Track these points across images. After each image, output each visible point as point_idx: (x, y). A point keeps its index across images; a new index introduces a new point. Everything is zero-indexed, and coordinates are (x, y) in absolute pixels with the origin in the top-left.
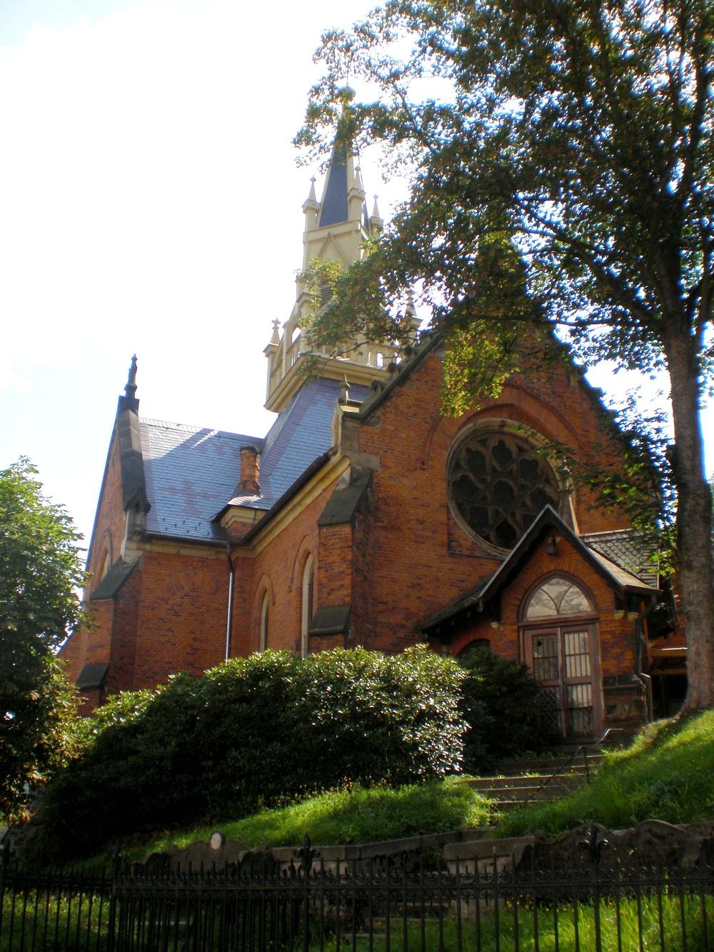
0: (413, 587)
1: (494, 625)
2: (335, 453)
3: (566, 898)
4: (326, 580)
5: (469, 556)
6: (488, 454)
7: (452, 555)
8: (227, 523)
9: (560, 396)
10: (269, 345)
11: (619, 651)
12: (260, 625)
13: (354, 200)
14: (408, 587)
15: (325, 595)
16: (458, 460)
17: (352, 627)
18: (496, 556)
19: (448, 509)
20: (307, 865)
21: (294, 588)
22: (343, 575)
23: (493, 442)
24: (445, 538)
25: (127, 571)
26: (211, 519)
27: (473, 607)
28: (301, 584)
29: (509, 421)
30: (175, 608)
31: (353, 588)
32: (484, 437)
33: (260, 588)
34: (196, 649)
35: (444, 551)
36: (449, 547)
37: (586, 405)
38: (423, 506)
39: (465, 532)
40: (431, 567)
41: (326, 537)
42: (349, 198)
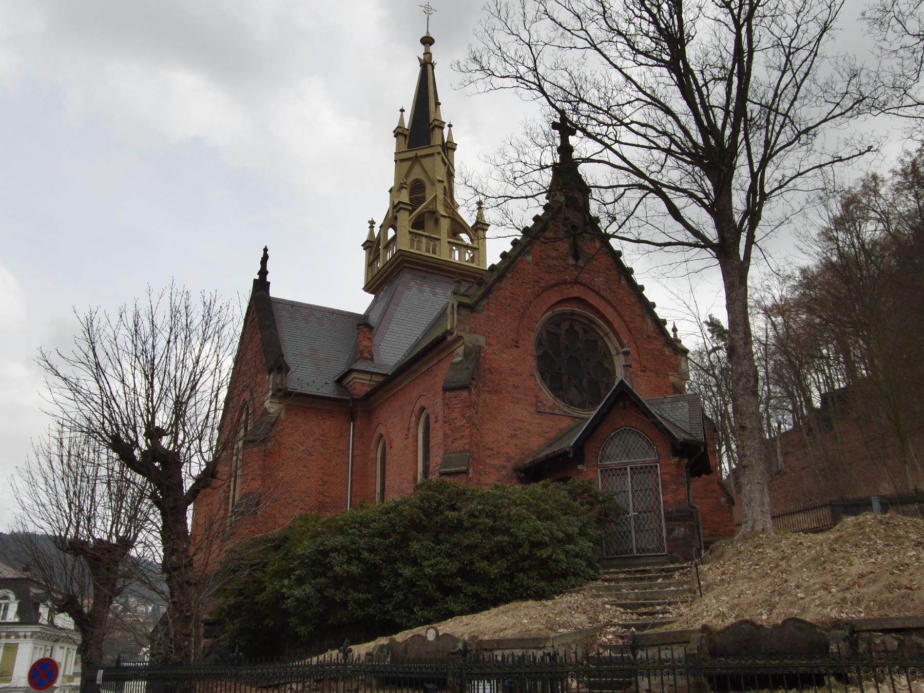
0: (511, 437)
1: (580, 467)
4: (450, 432)
5: (551, 414)
7: (540, 413)
8: (348, 383)
9: (614, 292)
17: (471, 468)
25: (273, 420)
26: (335, 379)
27: (565, 453)
28: (417, 433)
34: (325, 482)
35: (532, 410)
37: (633, 299)
40: (524, 422)
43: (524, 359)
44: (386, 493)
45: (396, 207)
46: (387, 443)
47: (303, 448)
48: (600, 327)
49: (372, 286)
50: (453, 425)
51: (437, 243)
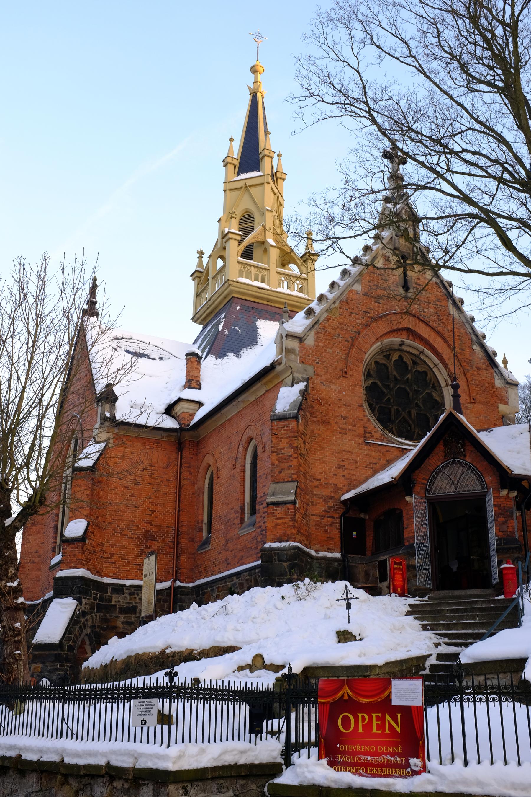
0: (339, 467)
1: (408, 499)
2: (280, 364)
4: (277, 462)
6: (391, 366)
9: (443, 323)
10: (196, 271)
11: (504, 519)
12: (203, 493)
13: (266, 158)
14: (336, 467)
15: (277, 473)
16: (369, 370)
19: (364, 408)
20: (171, 680)
22: (291, 458)
23: (395, 357)
24: (362, 431)
28: (245, 463)
29: (407, 341)
30: (137, 479)
32: (388, 353)
33: (204, 464)
35: (361, 440)
38: (345, 405)
39: (375, 425)
40: (352, 453)
41: (277, 429)
42: (261, 156)
43: (353, 389)
46: (214, 473)
47: (131, 477)
49: (198, 319)
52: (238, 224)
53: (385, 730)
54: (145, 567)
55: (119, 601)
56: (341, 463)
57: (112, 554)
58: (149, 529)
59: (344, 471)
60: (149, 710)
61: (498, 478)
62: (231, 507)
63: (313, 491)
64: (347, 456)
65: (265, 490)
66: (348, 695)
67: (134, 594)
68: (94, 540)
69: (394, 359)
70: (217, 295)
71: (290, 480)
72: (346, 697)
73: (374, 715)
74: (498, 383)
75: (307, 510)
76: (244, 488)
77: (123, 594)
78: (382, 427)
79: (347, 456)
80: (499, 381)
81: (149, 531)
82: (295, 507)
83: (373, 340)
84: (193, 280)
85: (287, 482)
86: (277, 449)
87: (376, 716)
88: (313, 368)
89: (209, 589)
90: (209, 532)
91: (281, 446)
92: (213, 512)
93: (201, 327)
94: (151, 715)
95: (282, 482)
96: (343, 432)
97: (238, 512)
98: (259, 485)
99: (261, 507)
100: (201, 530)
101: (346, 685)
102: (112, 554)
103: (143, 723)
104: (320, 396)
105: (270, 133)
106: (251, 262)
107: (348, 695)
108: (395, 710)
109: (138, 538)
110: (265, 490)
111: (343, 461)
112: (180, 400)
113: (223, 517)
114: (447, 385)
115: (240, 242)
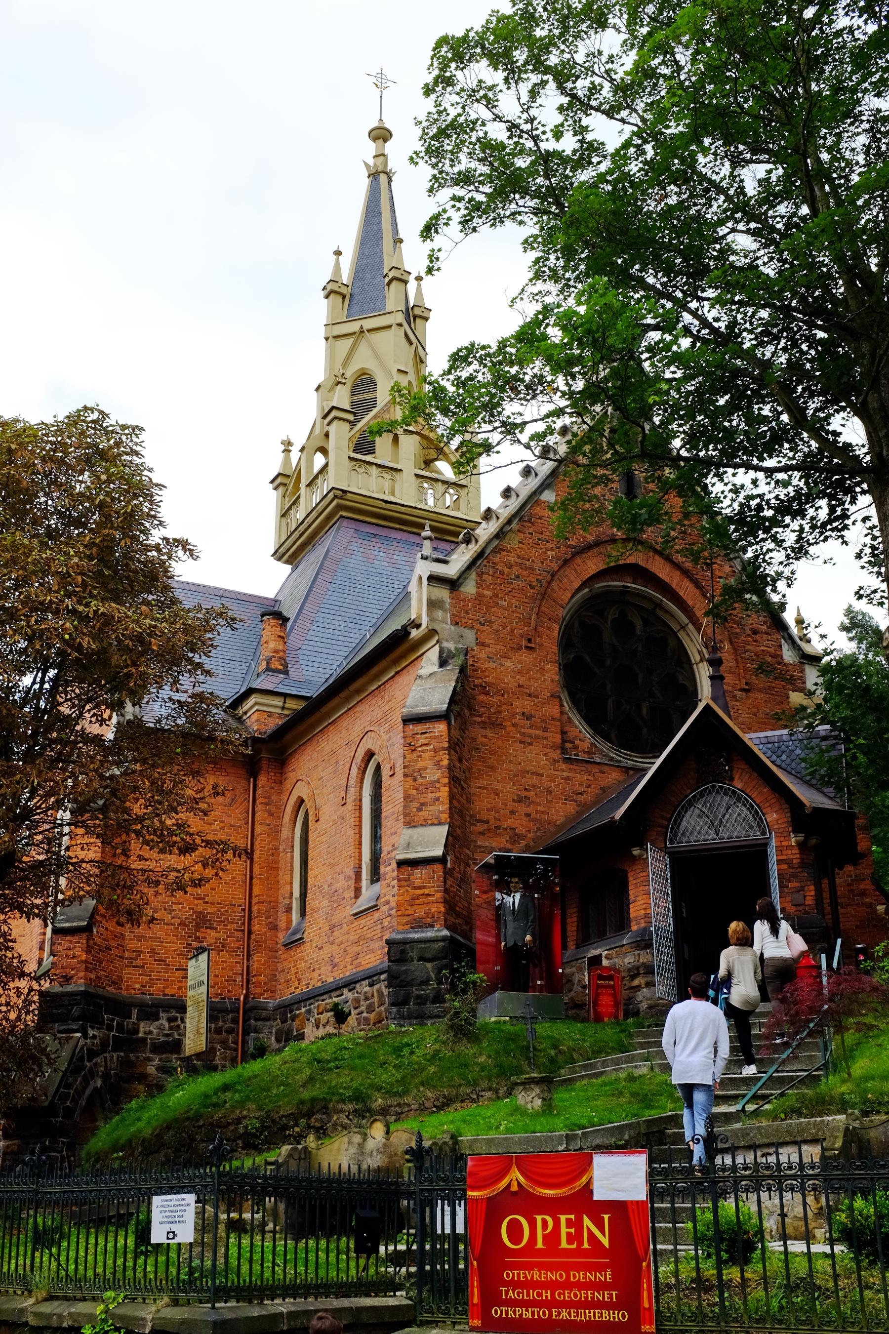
0: (520, 800)
1: (636, 852)
3: (359, 1182)
4: (414, 792)
7: (567, 760)
10: (279, 475)
11: (798, 884)
18: (620, 761)
19: (561, 700)
21: (350, 799)
22: (437, 785)
24: (558, 739)
28: (361, 795)
31: (451, 802)
35: (556, 755)
36: (564, 750)
38: (530, 695)
39: (581, 729)
40: (542, 776)
44: (309, 896)
45: (329, 414)
48: (672, 616)
49: (284, 554)
50: (419, 781)
51: (397, 476)
52: (349, 394)
53: (583, 1244)
54: (191, 972)
55: (150, 1032)
56: (524, 794)
57: (138, 953)
58: (200, 908)
59: (528, 806)
60: (180, 1213)
61: (788, 815)
62: (338, 869)
63: (476, 842)
64: (534, 780)
65: (393, 839)
66: (519, 1184)
67: (175, 1019)
68: (107, 929)
69: (610, 617)
70: (314, 514)
71: (436, 822)
72: (514, 1188)
73: (563, 1218)
74: (788, 655)
75: (465, 873)
76: (361, 837)
77: (158, 1019)
78: (591, 732)
79: (534, 780)
80: (790, 653)
81: (202, 913)
82: (445, 867)
83: (576, 585)
84: (276, 489)
85: (432, 825)
86: (414, 771)
87: (568, 1220)
88: (474, 632)
89: (303, 1010)
90: (303, 913)
91: (420, 764)
92: (309, 880)
93: (288, 568)
94: (185, 1222)
95: (422, 825)
96: (526, 742)
97: (350, 878)
98: (385, 832)
99: (389, 868)
100: (289, 910)
101: (514, 1168)
102: (138, 953)
103: (171, 1236)
104: (487, 680)
105: (401, 241)
106: (369, 458)
107: (519, 1184)
108: (597, 1209)
109: (183, 924)
110: (393, 839)
111: (526, 789)
112: (250, 692)
113: (326, 887)
114: (701, 661)
115: (352, 424)
